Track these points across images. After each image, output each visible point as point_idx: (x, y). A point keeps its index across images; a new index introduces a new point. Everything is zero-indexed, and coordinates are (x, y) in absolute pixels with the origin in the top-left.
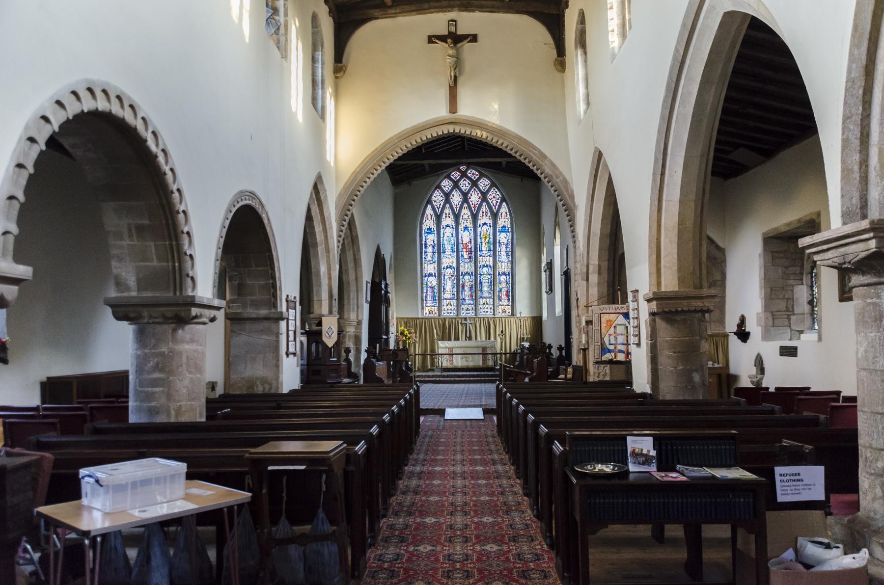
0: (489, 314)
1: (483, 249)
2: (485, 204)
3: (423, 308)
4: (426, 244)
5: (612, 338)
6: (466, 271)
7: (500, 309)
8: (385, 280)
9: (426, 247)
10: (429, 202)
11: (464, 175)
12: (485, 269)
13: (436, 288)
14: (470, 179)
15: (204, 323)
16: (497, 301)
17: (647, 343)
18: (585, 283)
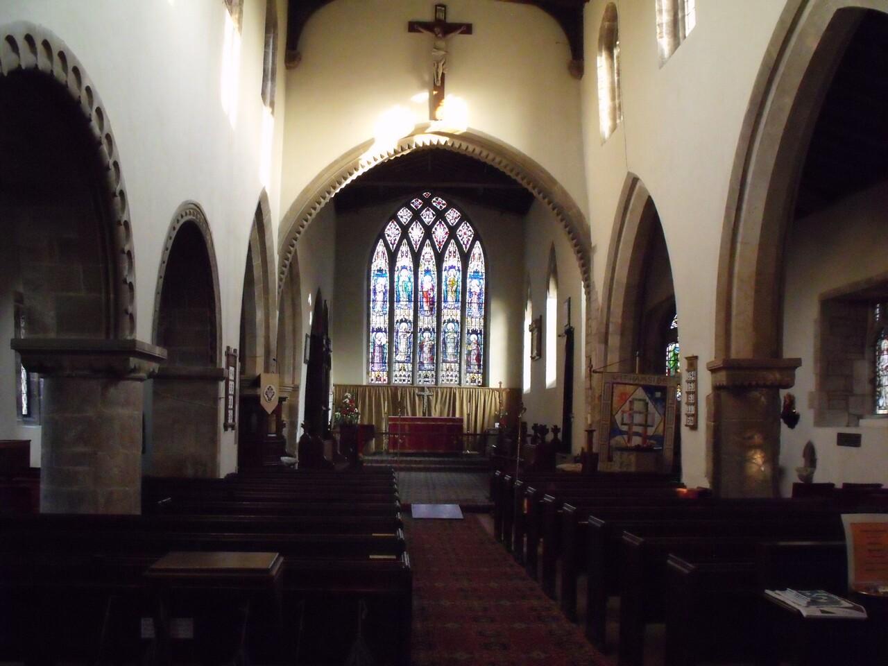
0: (454, 383)
1: (449, 299)
2: (453, 241)
3: (368, 373)
4: (375, 290)
5: (626, 416)
6: (425, 326)
8: (327, 335)
9: (375, 293)
10: (382, 236)
11: (427, 204)
12: (451, 326)
13: (386, 347)
14: (434, 208)
15: (141, 380)
17: (708, 426)
18: (603, 347)
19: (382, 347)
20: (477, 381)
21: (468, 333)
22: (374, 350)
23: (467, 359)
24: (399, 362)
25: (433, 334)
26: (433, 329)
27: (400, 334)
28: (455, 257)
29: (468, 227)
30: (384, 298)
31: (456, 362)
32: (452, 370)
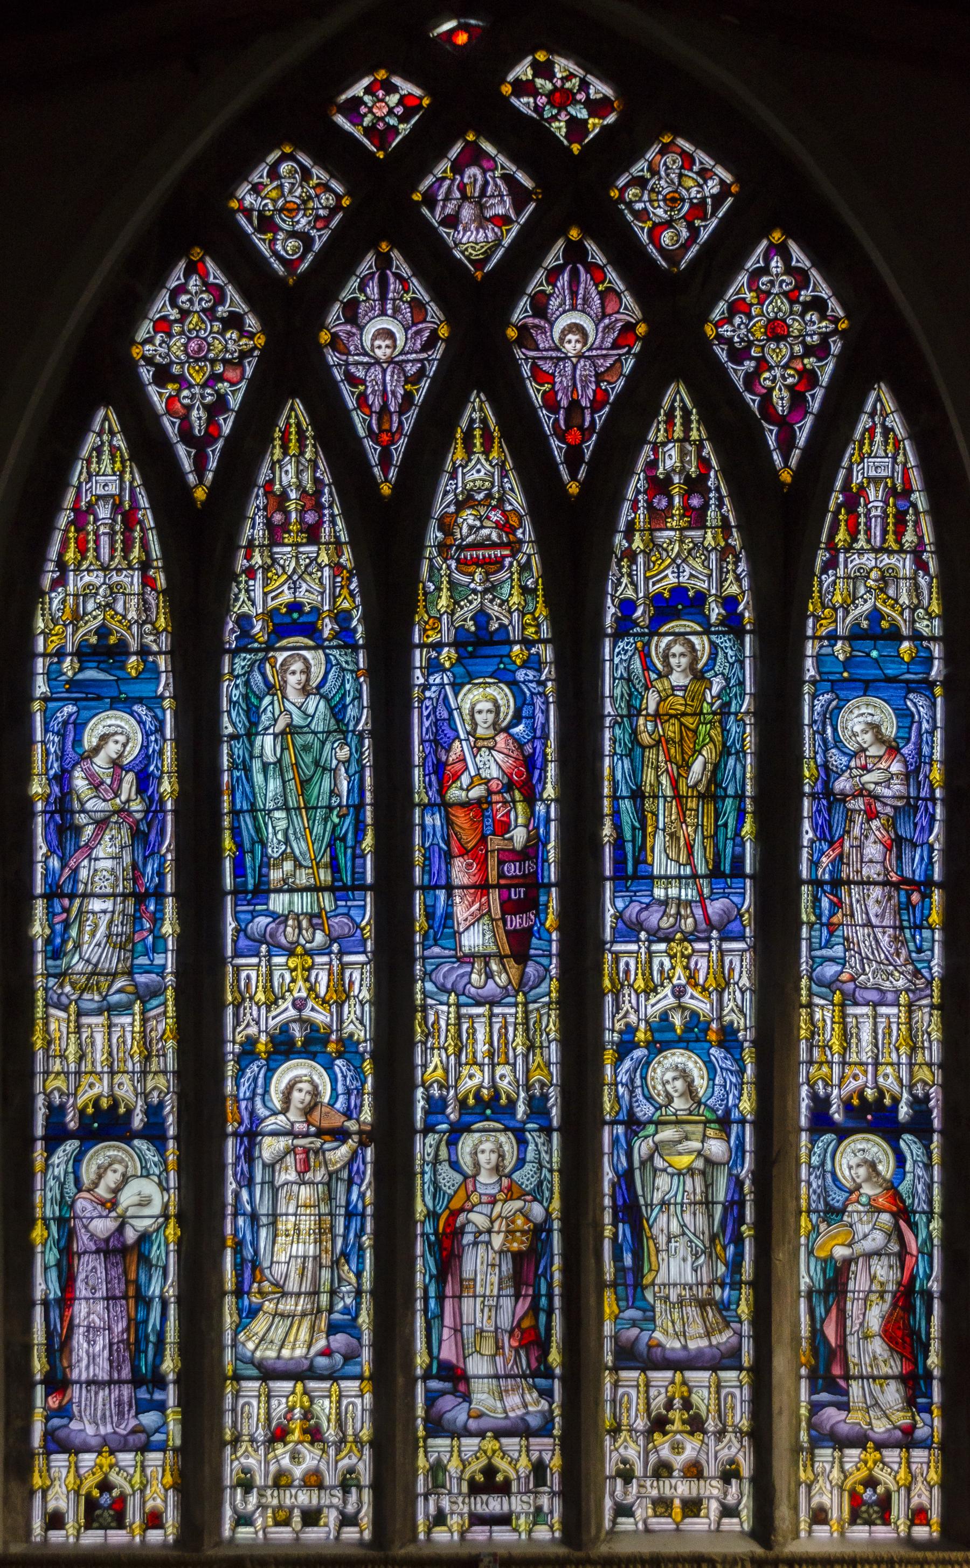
2: (676, 395)
4: (63, 804)
6: (474, 1080)
7: (826, 1481)
9: (65, 831)
10: (104, 375)
11: (465, 104)
12: (674, 1069)
13: (165, 1251)
14: (527, 141)
16: (795, 1394)
19: (124, 1252)
20: (899, 1510)
21: (821, 1121)
22: (68, 1281)
23: (817, 1333)
24: (268, 1373)
25: (535, 1139)
26: (538, 1107)
27: (270, 1148)
28: (697, 519)
29: (751, 380)
30: (136, 870)
31: (727, 1359)
32: (696, 1425)
